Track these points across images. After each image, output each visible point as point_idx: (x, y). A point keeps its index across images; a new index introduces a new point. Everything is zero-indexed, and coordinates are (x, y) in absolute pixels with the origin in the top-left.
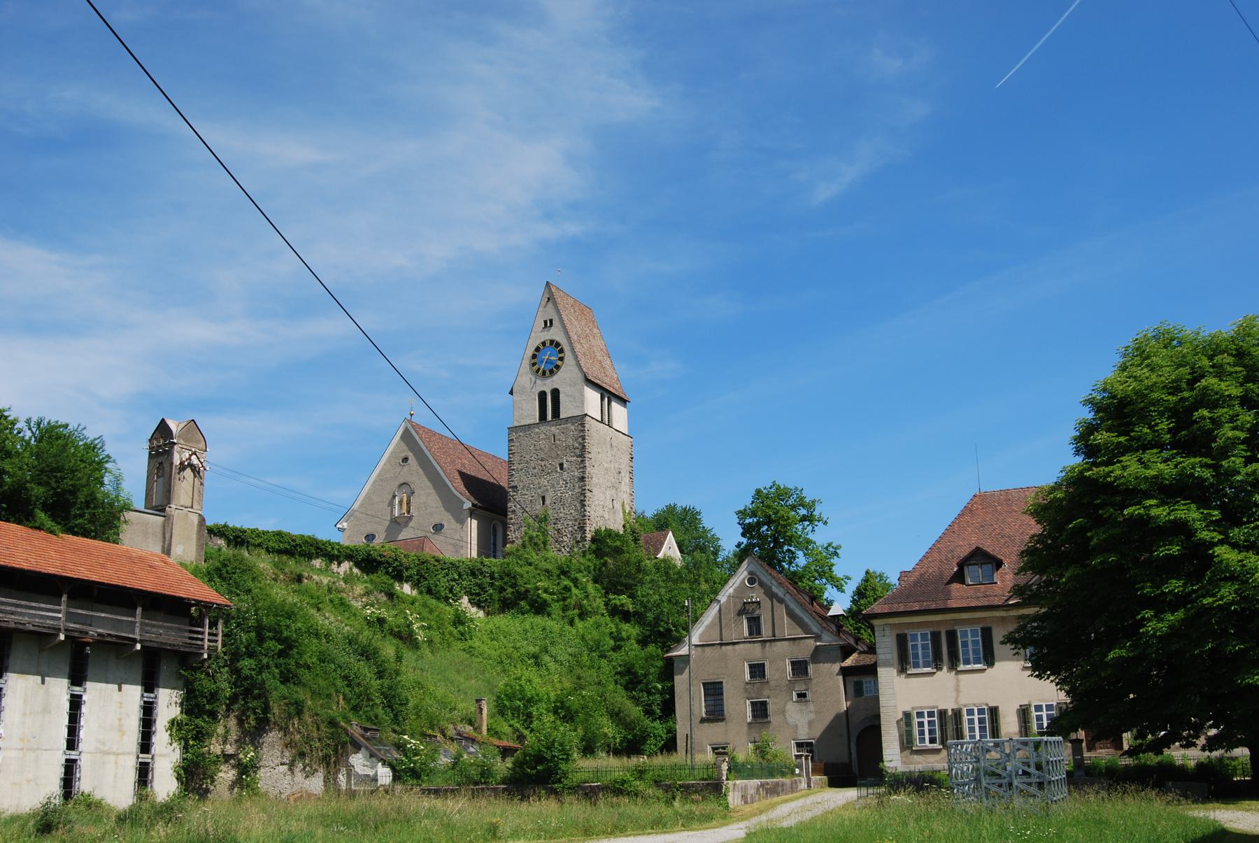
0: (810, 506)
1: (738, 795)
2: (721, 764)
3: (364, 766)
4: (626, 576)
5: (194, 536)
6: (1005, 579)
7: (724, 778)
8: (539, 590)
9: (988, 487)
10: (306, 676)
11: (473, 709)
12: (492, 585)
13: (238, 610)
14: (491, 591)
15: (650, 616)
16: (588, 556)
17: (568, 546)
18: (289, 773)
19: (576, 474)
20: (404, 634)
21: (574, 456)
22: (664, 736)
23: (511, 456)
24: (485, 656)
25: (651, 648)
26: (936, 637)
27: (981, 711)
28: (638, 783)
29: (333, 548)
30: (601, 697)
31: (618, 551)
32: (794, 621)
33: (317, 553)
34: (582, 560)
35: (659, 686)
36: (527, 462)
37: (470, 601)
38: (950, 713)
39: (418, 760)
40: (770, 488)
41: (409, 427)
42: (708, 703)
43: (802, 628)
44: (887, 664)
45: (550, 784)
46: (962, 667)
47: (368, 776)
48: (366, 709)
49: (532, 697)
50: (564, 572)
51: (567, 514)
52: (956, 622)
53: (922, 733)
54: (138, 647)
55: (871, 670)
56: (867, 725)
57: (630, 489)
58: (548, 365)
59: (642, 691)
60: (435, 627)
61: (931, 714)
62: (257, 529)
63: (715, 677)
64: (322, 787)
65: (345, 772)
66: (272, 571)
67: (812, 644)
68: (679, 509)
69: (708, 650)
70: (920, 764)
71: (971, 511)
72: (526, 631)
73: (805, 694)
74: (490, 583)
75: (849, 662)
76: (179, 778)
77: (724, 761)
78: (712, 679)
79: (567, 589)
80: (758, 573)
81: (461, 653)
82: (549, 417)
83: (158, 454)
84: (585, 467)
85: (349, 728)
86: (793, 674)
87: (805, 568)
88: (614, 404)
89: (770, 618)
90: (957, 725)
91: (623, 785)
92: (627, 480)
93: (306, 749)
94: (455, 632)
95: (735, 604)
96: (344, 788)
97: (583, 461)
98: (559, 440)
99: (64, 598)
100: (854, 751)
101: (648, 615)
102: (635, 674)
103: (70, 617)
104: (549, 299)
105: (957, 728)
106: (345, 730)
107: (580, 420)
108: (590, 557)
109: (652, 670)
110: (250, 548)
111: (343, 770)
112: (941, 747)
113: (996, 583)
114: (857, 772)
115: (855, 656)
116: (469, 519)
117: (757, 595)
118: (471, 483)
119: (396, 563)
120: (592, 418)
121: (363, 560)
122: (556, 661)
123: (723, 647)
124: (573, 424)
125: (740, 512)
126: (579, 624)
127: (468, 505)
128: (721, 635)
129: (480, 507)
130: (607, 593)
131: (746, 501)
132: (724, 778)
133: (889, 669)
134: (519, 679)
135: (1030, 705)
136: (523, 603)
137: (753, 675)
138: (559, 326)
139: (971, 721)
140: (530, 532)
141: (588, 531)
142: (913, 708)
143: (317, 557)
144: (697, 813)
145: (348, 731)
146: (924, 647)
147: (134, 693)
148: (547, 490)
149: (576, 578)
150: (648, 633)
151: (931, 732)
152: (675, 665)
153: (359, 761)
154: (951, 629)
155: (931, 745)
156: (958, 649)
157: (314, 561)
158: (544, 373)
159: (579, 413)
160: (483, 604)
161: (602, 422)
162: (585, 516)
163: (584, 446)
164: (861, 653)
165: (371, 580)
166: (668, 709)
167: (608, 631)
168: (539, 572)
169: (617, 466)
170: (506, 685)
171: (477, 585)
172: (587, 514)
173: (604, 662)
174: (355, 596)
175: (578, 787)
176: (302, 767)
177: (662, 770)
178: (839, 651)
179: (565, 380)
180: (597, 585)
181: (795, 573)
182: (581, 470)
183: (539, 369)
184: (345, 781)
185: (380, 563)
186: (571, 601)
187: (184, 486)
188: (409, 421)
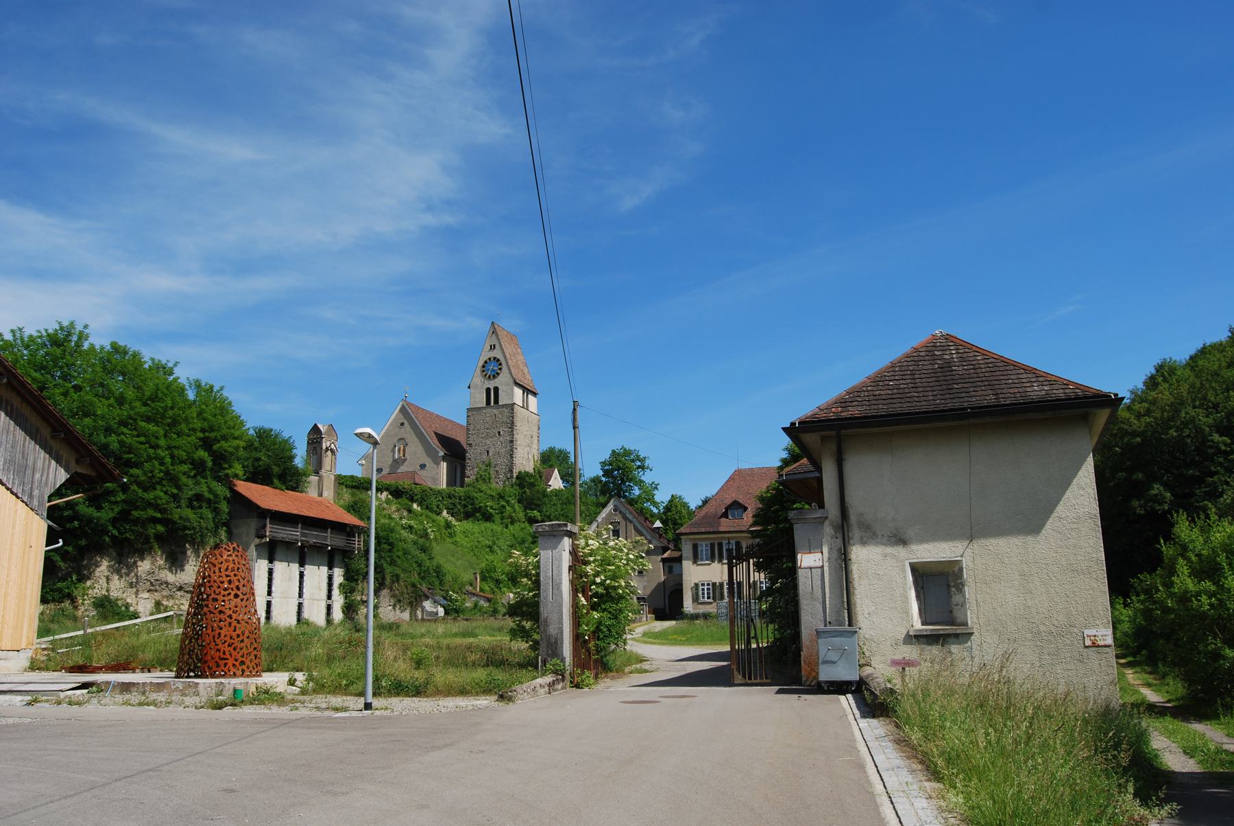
0: (643, 460)
5: (332, 486)
6: (748, 518)
10: (399, 562)
11: (472, 578)
12: (460, 503)
13: (1113, 707)
14: (459, 507)
19: (508, 438)
26: (712, 545)
31: (532, 485)
38: (718, 584)
41: (405, 404)
44: (687, 559)
50: (501, 497)
51: (502, 462)
52: (723, 538)
53: (703, 594)
54: (329, 548)
55: (679, 560)
70: (702, 609)
71: (733, 479)
75: (666, 555)
76: (343, 612)
79: (503, 507)
82: (492, 404)
83: (313, 442)
84: (513, 435)
87: (639, 496)
88: (529, 396)
92: (536, 441)
94: (446, 532)
99: (300, 525)
103: (303, 535)
107: (512, 406)
111: (420, 609)
115: (669, 552)
117: (618, 518)
118: (445, 441)
122: (501, 549)
125: (602, 462)
126: (511, 527)
127: (441, 454)
131: (606, 456)
136: (478, 515)
140: (481, 472)
142: (700, 581)
147: (324, 570)
151: (708, 594)
153: (428, 605)
159: (510, 402)
164: (672, 550)
165: (399, 503)
171: (452, 503)
179: (502, 381)
181: (632, 499)
185: (403, 492)
186: (506, 514)
187: (327, 460)
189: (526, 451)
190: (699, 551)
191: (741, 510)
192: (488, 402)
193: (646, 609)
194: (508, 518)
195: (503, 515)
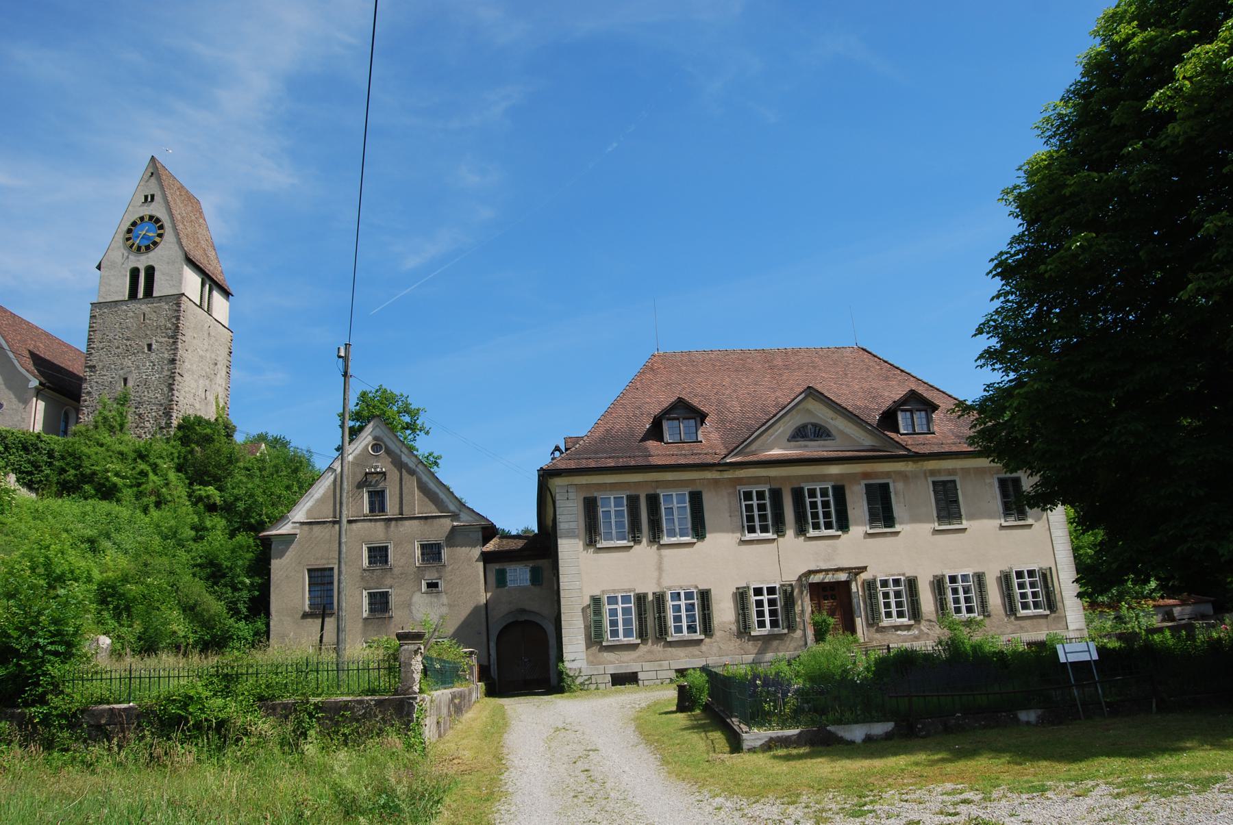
0: (414, 414)
2: (411, 659)
7: (416, 689)
8: (108, 472)
9: (668, 348)
12: (50, 464)
14: (49, 472)
15: (241, 506)
16: (172, 442)
17: (150, 432)
19: (166, 355)
21: (165, 337)
22: (250, 639)
23: (92, 333)
25: (241, 538)
26: (633, 502)
27: (689, 596)
28: (220, 702)
30: (172, 586)
31: (208, 439)
32: (427, 497)
34: (164, 446)
35: (247, 581)
36: (110, 341)
37: (18, 480)
38: (650, 598)
40: (377, 391)
42: (313, 593)
43: (436, 506)
44: (571, 535)
45: (18, 707)
46: (665, 540)
49: (63, 574)
50: (142, 456)
56: (511, 621)
57: (226, 384)
58: (145, 241)
59: (225, 585)
61: (626, 599)
63: (324, 561)
67: (447, 524)
69: (316, 528)
72: (85, 514)
73: (437, 583)
74: (47, 462)
75: (491, 546)
77: (416, 652)
78: (321, 563)
79: (144, 474)
80: (386, 439)
82: (141, 294)
86: (423, 560)
90: (659, 613)
91: (185, 706)
92: (223, 373)
97: (175, 343)
101: (239, 504)
102: (219, 566)
104: (152, 174)
105: (660, 617)
107: (177, 299)
108: (175, 443)
109: (240, 563)
112: (639, 641)
113: (701, 442)
114: (496, 677)
116: (35, 399)
118: (40, 363)
120: (190, 300)
124: (167, 303)
126: (155, 514)
127: (34, 383)
129: (49, 388)
130: (191, 484)
132: (416, 689)
133: (573, 541)
134: (48, 547)
135: (748, 587)
136: (87, 487)
137: (372, 559)
138: (161, 201)
141: (174, 417)
142: (603, 592)
146: (619, 514)
149: (155, 464)
150: (236, 525)
152: (273, 546)
154: (653, 492)
155: (626, 639)
156: (661, 518)
159: (176, 292)
160: (36, 486)
161: (200, 306)
162: (172, 400)
163: (178, 327)
166: (260, 606)
168: (111, 453)
169: (213, 356)
171: (29, 462)
173: (181, 553)
175: (83, 712)
177: (277, 674)
179: (164, 257)
180: (180, 474)
182: (172, 352)
183: (133, 244)
189: (201, 386)
190: (600, 515)
191: (692, 422)
192: (133, 294)
194: (151, 494)
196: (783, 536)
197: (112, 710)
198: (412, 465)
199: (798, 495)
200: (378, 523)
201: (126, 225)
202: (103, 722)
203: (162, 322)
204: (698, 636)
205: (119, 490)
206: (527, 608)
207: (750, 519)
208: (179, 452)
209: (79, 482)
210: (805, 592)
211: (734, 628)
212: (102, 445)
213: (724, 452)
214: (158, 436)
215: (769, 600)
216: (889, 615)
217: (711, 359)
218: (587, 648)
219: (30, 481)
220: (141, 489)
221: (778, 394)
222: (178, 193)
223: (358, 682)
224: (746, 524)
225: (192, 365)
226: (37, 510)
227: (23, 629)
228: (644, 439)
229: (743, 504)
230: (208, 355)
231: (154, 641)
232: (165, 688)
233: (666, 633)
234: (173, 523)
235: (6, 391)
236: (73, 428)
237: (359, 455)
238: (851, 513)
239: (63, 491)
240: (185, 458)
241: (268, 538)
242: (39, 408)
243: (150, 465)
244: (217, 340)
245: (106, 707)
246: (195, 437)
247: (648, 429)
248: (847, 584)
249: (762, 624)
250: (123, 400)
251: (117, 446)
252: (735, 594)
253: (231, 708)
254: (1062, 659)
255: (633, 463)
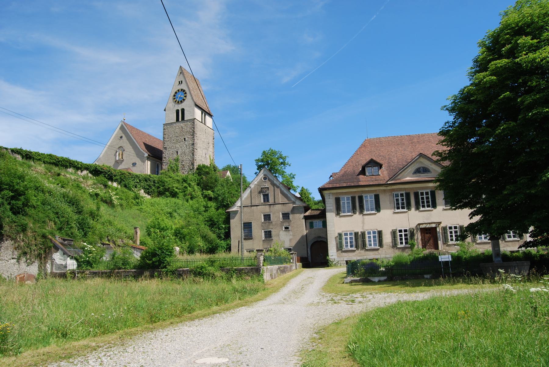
1: (269, 274)
2: (260, 257)
3: (60, 259)
4: (211, 183)
7: (262, 265)
10: (31, 211)
12: (154, 185)
15: (220, 198)
16: (195, 175)
18: (17, 263)
19: (191, 142)
20: (108, 201)
22: (225, 247)
24: (147, 212)
25: (220, 211)
26: (353, 199)
27: (374, 233)
28: (210, 268)
29: (78, 164)
30: (198, 229)
31: (207, 173)
33: (70, 166)
34: (192, 176)
35: (224, 226)
37: (144, 192)
38: (360, 233)
39: (91, 256)
40: (269, 151)
42: (245, 231)
44: (331, 211)
45: (160, 269)
46: (365, 212)
47: (62, 265)
48: (66, 229)
49: (164, 227)
50: (185, 181)
51: (186, 159)
53: (347, 243)
58: (180, 99)
59: (216, 228)
60: (124, 199)
61: (351, 234)
62: (39, 152)
63: (248, 220)
64: (37, 271)
65: (50, 263)
66: (44, 171)
67: (291, 206)
68: (232, 167)
71: (365, 146)
72: (167, 203)
75: (307, 213)
77: (261, 255)
79: (186, 187)
80: (268, 175)
81: (137, 211)
82: (180, 120)
85: (53, 239)
86: (283, 219)
89: (273, 194)
90: (363, 239)
91: (201, 269)
92: (212, 147)
93: (28, 250)
94: (134, 202)
95: (258, 188)
96: (50, 271)
98: (184, 129)
100: (309, 252)
101: (219, 198)
102: (213, 221)
105: (363, 241)
106: (51, 240)
107: (193, 120)
109: (221, 219)
110: (34, 161)
111: (49, 262)
112: (356, 249)
113: (380, 175)
114: (310, 261)
115: (309, 211)
117: (267, 184)
118: (149, 148)
119: (109, 173)
121: (93, 170)
122: (179, 215)
123: (252, 207)
124: (190, 122)
125: (257, 160)
126: (191, 202)
127: (146, 155)
128: (251, 202)
129: (151, 156)
130: (202, 190)
132: (262, 265)
134: (158, 219)
135: (396, 230)
136: (167, 193)
138: (185, 83)
139: (370, 237)
141: (195, 165)
143: (70, 167)
144: (248, 288)
145: (52, 240)
148: (179, 149)
149: (190, 183)
150: (219, 205)
151: (351, 242)
152: (231, 215)
153: (57, 257)
156: (364, 204)
157: (68, 169)
158: (178, 102)
159: (192, 118)
160: (150, 193)
161: (202, 122)
162: (194, 159)
166: (228, 235)
167: (202, 204)
168: (174, 180)
169: (208, 141)
170: (151, 222)
171: (147, 185)
172: (195, 158)
173: (200, 216)
174: (88, 185)
175: (176, 270)
176: (25, 260)
177: (225, 261)
178: (303, 209)
179: (187, 105)
182: (193, 141)
183: (176, 101)
184: (50, 267)
185: (101, 172)
186: (188, 192)
188: (123, 122)
190: (341, 204)
191: (377, 167)
193: (295, 257)
195: (185, 193)
196: (410, 210)
197: (183, 270)
198: (278, 184)
199: (416, 195)
200: (267, 206)
201: (173, 94)
202: (181, 273)
203: (188, 129)
204: (377, 247)
205: (178, 194)
206: (321, 236)
207: (398, 204)
208: (198, 178)
209: (164, 191)
210: (418, 231)
211: (391, 244)
212: (171, 177)
213: (388, 179)
214: (190, 173)
215: (404, 234)
216: (452, 240)
217: (388, 140)
218: (337, 251)
219: (148, 192)
220: (185, 193)
221: (413, 154)
222: (191, 79)
223: (246, 263)
224: (396, 206)
225: (200, 145)
226: (152, 203)
227: (159, 249)
228: (358, 175)
229: (395, 198)
230: (206, 140)
231: (193, 249)
232: (196, 264)
233: (366, 246)
234: (197, 205)
235: (137, 158)
236: (161, 172)
237: (259, 181)
238: (438, 201)
239: (159, 195)
240: (200, 180)
241: (229, 212)
242: (148, 163)
243: (188, 184)
244: (208, 134)
245: (182, 269)
246: (203, 172)
247: (361, 171)
248: (435, 228)
249: (402, 243)
250: (177, 160)
251: (176, 177)
252: (391, 232)
253: (211, 269)
254: (440, 260)
255: (353, 185)
